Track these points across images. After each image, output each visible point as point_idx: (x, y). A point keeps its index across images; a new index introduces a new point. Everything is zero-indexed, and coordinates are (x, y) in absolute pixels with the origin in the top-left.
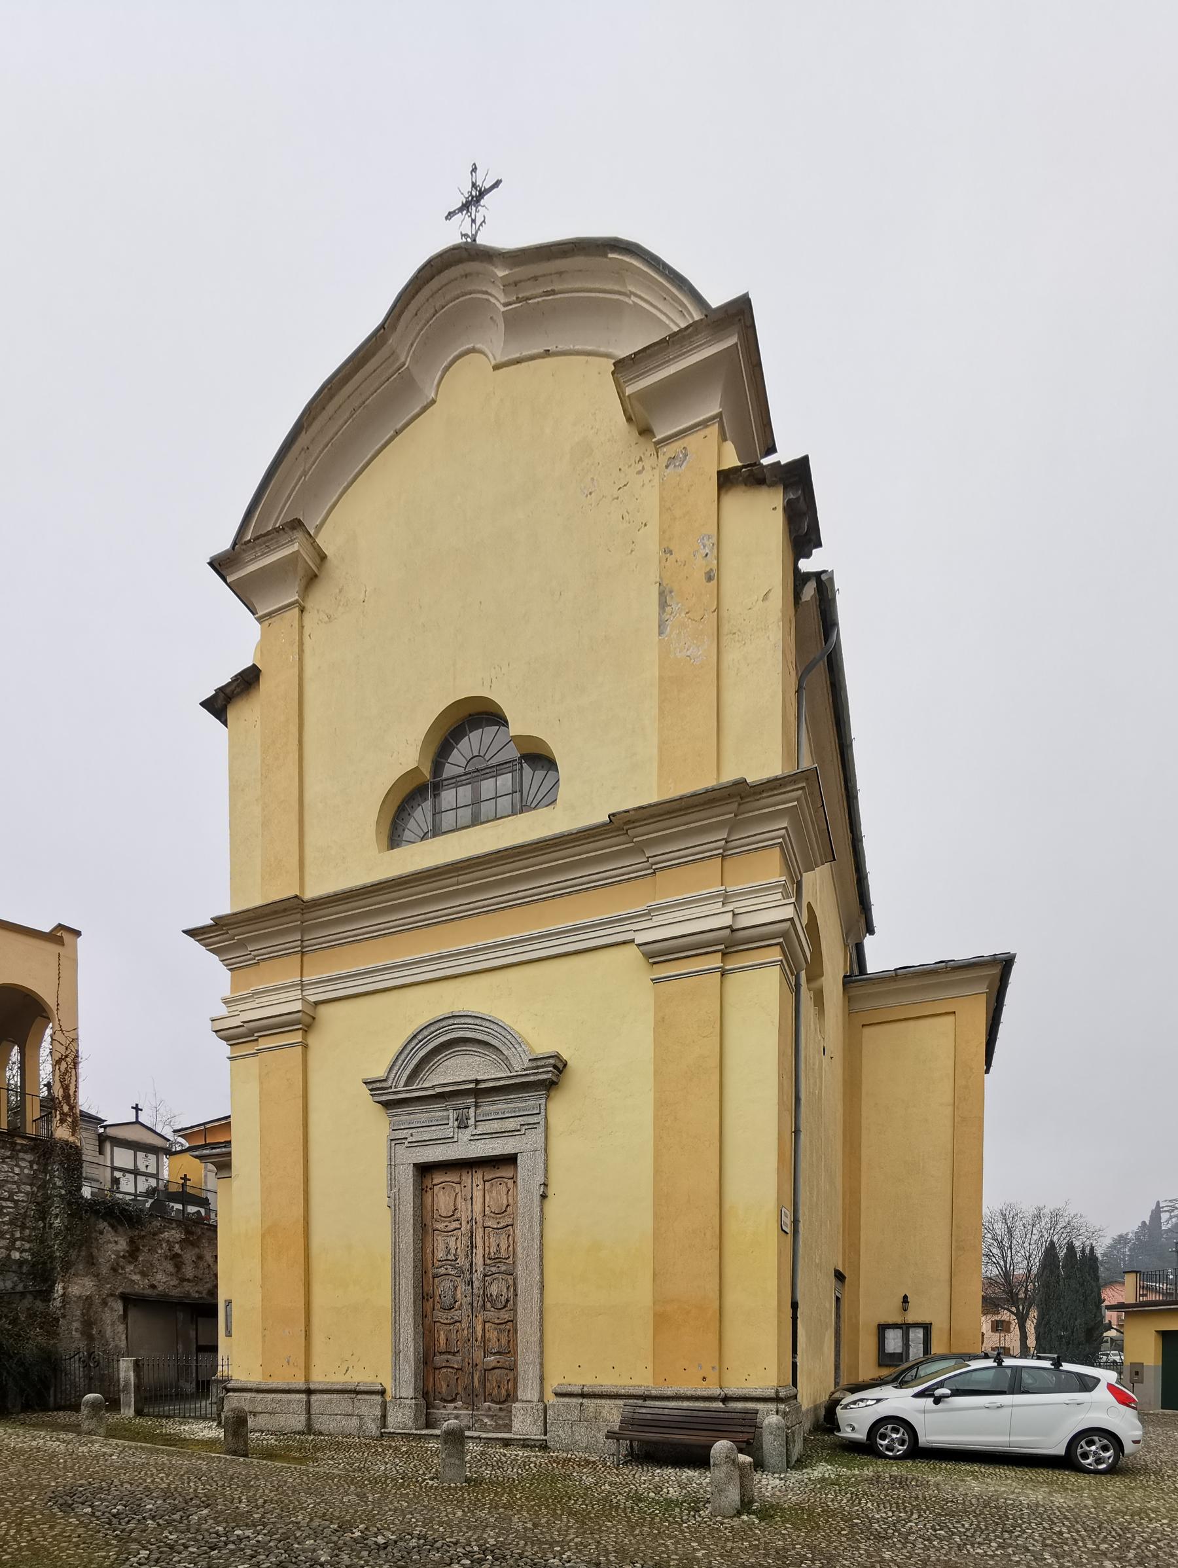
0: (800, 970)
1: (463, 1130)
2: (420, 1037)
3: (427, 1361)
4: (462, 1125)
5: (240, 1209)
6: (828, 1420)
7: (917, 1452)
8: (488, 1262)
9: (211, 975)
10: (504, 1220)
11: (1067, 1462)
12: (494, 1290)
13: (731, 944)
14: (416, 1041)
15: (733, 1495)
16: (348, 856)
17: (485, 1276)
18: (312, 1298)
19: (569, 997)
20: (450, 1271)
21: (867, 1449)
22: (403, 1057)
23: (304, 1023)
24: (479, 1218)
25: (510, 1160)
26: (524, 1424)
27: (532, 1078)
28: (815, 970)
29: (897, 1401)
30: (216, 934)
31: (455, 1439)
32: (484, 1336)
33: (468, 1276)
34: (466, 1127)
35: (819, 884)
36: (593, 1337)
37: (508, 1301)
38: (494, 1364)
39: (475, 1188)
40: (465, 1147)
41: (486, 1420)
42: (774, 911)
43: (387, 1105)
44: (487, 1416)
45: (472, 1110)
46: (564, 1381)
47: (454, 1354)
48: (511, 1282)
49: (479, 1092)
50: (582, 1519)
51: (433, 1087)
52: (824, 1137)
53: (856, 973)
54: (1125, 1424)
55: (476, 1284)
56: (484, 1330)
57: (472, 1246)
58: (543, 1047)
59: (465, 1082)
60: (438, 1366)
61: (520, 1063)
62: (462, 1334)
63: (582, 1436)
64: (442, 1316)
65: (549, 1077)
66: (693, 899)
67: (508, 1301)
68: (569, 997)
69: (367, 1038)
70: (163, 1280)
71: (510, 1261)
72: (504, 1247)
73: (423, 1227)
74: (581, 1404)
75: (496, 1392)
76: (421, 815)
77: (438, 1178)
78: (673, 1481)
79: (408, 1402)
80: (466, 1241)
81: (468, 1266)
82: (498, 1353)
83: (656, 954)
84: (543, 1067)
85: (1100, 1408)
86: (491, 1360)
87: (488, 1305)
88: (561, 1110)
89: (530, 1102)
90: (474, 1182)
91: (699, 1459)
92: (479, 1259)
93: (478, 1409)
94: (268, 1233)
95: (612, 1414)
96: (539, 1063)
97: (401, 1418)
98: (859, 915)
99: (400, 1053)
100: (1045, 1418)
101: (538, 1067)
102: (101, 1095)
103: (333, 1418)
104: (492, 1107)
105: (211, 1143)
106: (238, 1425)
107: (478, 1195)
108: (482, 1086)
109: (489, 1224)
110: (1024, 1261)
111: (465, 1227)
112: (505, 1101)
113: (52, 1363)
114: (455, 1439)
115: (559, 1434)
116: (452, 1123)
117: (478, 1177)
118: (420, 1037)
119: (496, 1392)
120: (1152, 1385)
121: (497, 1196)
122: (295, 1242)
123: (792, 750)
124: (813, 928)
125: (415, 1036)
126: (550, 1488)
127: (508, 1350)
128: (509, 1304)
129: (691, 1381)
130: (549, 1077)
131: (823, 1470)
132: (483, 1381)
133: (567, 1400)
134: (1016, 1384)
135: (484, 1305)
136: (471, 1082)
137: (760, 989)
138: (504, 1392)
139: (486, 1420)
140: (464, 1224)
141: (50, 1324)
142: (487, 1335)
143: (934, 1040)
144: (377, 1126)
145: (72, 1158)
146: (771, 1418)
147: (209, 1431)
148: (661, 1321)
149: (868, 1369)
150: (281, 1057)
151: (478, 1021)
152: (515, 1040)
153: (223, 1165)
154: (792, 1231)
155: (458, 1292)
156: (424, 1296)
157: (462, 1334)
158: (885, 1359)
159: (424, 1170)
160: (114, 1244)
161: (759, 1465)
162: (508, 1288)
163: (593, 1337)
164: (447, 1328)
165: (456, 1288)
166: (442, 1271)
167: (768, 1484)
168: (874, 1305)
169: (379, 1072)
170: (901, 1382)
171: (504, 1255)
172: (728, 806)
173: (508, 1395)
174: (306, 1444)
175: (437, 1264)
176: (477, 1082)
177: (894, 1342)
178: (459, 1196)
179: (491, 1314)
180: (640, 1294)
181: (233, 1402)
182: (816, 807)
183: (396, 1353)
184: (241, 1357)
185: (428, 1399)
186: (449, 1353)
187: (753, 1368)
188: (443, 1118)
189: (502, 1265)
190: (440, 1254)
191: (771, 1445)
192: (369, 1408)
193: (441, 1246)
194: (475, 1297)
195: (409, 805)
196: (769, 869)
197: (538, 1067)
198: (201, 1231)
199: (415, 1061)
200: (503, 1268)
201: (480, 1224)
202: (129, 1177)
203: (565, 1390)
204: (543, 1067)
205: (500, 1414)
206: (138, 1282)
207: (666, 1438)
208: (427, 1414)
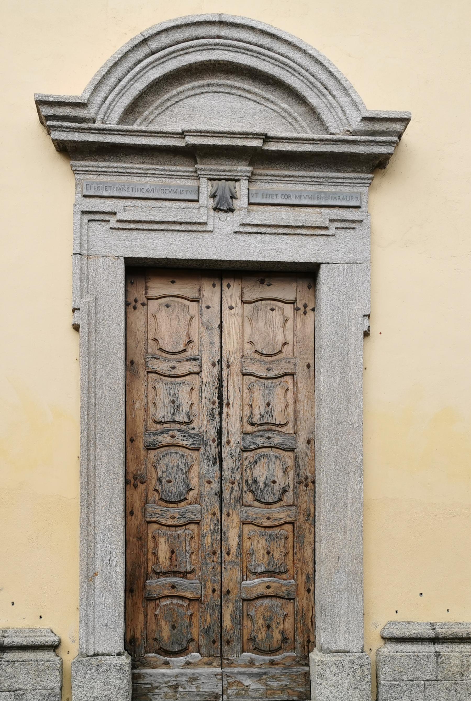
1: (223, 215)
2: (154, 45)
4: (224, 206)
8: (249, 428)
10: (286, 369)
12: (260, 473)
14: (144, 50)
17: (245, 450)
20: (179, 440)
22: (120, 71)
24: (235, 361)
25: (307, 274)
27: (361, 149)
32: (240, 546)
33: (213, 450)
34: (231, 210)
37: (284, 491)
38: (261, 590)
39: (226, 311)
40: (222, 242)
41: (247, 682)
43: (66, 150)
44: (251, 675)
45: (244, 184)
46: (396, 617)
47: (185, 575)
48: (290, 462)
49: (262, 157)
51: (182, 135)
55: (228, 463)
56: (241, 536)
57: (221, 401)
59: (246, 135)
60: (154, 594)
64: (167, 514)
65: (368, 157)
67: (284, 491)
71: (290, 429)
72: (278, 407)
74: (438, 654)
75: (262, 635)
77: (158, 288)
79: (116, 660)
80: (210, 393)
81: (213, 433)
82: (269, 573)
84: (382, 133)
86: (256, 584)
87: (249, 497)
89: (339, 187)
92: (233, 423)
93: (230, 665)
96: (378, 127)
99: (116, 64)
101: (374, 133)
107: (232, 322)
108: (273, 147)
109: (253, 369)
111: (209, 373)
112: (302, 180)
116: (205, 200)
117: (233, 292)
118: (154, 45)
119: (262, 635)
125: (145, 41)
130: (368, 157)
132: (238, 620)
133: (408, 647)
135: (241, 498)
136: (256, 136)
138: (277, 636)
139: (247, 682)
140: (206, 367)
142: (247, 544)
151: (266, 41)
155: (194, 473)
159: (139, 270)
162: (285, 471)
164: (173, 532)
165: (190, 468)
166: (165, 439)
169: (74, 87)
171: (278, 418)
173: (285, 640)
175: (155, 427)
176: (267, 138)
178: (196, 321)
179: (258, 511)
183: (90, 577)
186: (175, 573)
188: (186, 190)
190: (162, 412)
194: (225, 484)
197: (374, 133)
199: (141, 85)
200: (277, 440)
201: (235, 369)
203: (398, 633)
204: (382, 133)
205: (273, 670)
208: (135, 678)
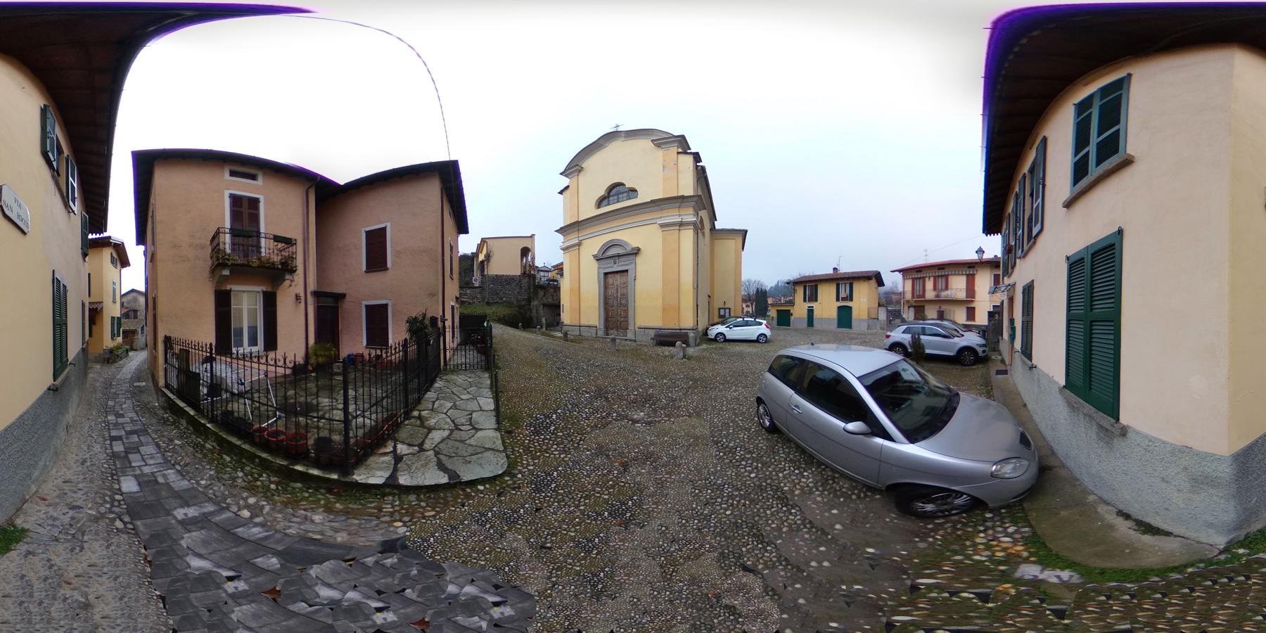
0: (698, 228)
3: (607, 320)
5: (565, 285)
6: (705, 333)
7: (726, 341)
9: (560, 237)
10: (625, 285)
11: (757, 341)
13: (681, 224)
15: (681, 354)
16: (589, 211)
18: (581, 302)
19: (639, 234)
21: (715, 340)
23: (579, 244)
26: (630, 335)
28: (703, 227)
29: (721, 329)
30: (562, 231)
31: (614, 340)
35: (704, 214)
36: (648, 313)
40: (616, 268)
42: (692, 219)
49: (619, 256)
50: (644, 361)
52: (705, 266)
53: (713, 228)
54: (768, 332)
58: (635, 245)
61: (629, 249)
62: (616, 310)
63: (644, 339)
65: (636, 252)
66: (672, 216)
68: (639, 234)
69: (593, 245)
70: (550, 300)
73: (606, 287)
76: (605, 202)
78: (667, 350)
83: (662, 226)
85: (763, 329)
88: (639, 259)
89: (632, 257)
90: (618, 276)
91: (673, 345)
94: (571, 290)
95: (652, 333)
97: (601, 333)
98: (713, 217)
100: (752, 332)
102: (539, 263)
103: (585, 333)
104: (623, 259)
105: (559, 268)
106: (566, 334)
110: (753, 291)
113: (531, 318)
114: (614, 340)
115: (638, 338)
120: (775, 321)
121: (623, 280)
122: (577, 291)
123: (695, 190)
124: (702, 221)
126: (636, 352)
127: (626, 317)
128: (626, 305)
129: (671, 324)
131: (704, 346)
134: (747, 324)
137: (688, 235)
141: (531, 310)
143: (732, 244)
144: (595, 265)
145: (534, 276)
146: (691, 334)
147: (559, 334)
148: (664, 310)
149: (716, 319)
150: (574, 252)
152: (627, 244)
153: (562, 275)
154: (696, 288)
156: (606, 303)
157: (616, 310)
158: (720, 317)
159: (606, 274)
160: (541, 293)
161: (688, 346)
163: (648, 313)
167: (690, 351)
168: (718, 304)
170: (723, 324)
172: (680, 200)
174: (579, 339)
177: (722, 313)
180: (659, 304)
181: (565, 328)
182: (703, 199)
184: (566, 317)
185: (607, 328)
187: (687, 321)
189: (625, 296)
191: (691, 341)
192: (593, 330)
193: (610, 292)
195: (600, 203)
196: (691, 211)
198: (557, 289)
202: (542, 278)
206: (545, 301)
207: (666, 339)
